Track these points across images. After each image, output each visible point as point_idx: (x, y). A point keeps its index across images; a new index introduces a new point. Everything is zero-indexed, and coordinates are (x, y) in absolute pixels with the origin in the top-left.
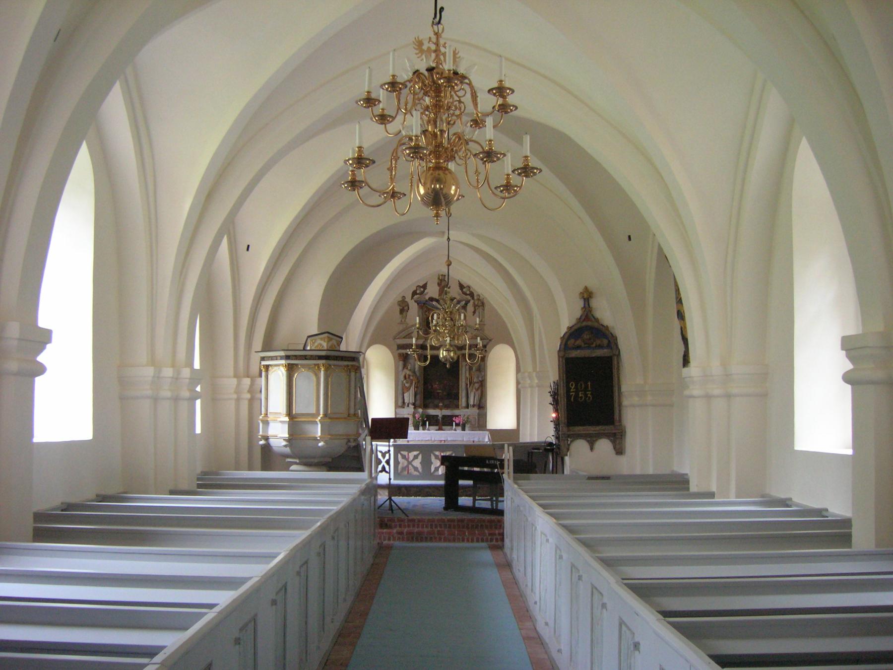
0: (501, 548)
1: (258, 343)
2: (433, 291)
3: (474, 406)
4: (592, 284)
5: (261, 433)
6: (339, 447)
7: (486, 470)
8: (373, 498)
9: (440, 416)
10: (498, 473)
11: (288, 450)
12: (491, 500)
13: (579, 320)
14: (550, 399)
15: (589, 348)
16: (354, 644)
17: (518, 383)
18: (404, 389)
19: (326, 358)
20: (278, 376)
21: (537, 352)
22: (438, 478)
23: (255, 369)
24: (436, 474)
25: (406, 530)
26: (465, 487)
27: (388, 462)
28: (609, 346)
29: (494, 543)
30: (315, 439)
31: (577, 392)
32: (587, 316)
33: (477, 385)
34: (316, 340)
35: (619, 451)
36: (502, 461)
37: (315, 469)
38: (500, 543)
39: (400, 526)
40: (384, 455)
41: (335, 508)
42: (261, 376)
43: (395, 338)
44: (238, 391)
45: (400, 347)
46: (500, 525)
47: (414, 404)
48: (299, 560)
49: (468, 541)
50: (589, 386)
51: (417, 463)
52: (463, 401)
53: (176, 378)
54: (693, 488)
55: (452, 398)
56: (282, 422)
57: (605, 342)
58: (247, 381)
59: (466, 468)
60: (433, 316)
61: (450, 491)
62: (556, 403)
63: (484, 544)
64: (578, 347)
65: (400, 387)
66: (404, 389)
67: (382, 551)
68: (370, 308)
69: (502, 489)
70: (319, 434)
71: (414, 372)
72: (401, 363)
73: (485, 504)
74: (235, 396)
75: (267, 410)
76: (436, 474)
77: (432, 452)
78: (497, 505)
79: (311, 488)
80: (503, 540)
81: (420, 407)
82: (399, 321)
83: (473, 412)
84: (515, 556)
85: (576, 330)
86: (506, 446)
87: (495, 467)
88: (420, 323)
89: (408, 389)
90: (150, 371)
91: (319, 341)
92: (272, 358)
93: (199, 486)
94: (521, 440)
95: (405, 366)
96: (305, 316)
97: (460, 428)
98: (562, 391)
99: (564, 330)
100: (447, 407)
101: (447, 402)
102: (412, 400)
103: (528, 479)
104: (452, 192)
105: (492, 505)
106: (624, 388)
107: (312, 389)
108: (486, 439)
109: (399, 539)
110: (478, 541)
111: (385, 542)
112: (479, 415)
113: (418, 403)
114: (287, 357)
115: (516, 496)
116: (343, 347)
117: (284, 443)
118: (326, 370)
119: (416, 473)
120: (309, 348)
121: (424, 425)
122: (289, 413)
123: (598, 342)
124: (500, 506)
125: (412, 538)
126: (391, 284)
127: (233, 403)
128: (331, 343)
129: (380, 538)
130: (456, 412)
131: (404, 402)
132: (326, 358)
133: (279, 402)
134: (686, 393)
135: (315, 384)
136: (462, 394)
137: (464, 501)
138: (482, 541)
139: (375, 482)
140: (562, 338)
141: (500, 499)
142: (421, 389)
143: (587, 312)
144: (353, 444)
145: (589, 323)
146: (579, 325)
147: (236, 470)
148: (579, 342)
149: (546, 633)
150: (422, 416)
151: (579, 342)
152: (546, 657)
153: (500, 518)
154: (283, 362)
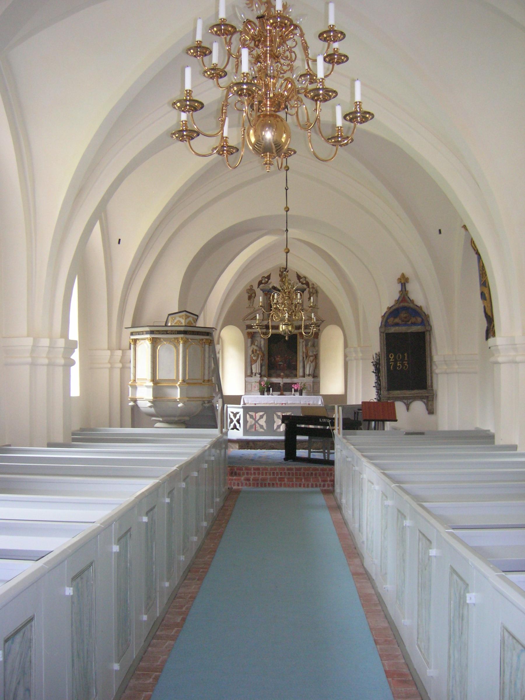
0: (332, 492)
1: (128, 321)
2: (275, 281)
3: (309, 375)
4: (409, 273)
5: (130, 396)
6: (196, 407)
7: (319, 427)
8: (223, 451)
9: (282, 384)
10: (329, 430)
11: (152, 410)
12: (324, 452)
13: (397, 301)
14: (373, 368)
15: (405, 325)
16: (201, 579)
17: (346, 356)
18: (252, 362)
19: (185, 332)
20: (144, 348)
21: (361, 329)
22: (279, 434)
23: (125, 342)
24: (278, 430)
25: (252, 477)
26: (302, 442)
27: (238, 421)
28: (422, 323)
29: (326, 488)
30: (175, 401)
31: (395, 361)
32: (404, 297)
33: (311, 358)
34: (175, 319)
35: (431, 411)
36: (333, 419)
37: (176, 426)
38: (331, 488)
39: (247, 474)
40: (235, 415)
41: (185, 459)
42: (130, 349)
44: (111, 362)
46: (331, 473)
47: (260, 374)
48: (148, 502)
49: (304, 486)
50: (406, 357)
51: (262, 422)
52: (300, 372)
53: (52, 347)
54: (499, 441)
55: (291, 369)
56: (148, 387)
57: (419, 320)
58: (119, 353)
59: (303, 426)
60: (273, 296)
61: (290, 445)
62: (377, 371)
63: (318, 489)
64: (397, 324)
65: (249, 360)
66: (252, 362)
67: (232, 495)
68: (224, 294)
69: (333, 444)
70: (179, 397)
73: (318, 455)
74: (109, 366)
75: (135, 376)
76: (278, 430)
77: (275, 413)
78: (328, 456)
79: (175, 442)
80: (333, 485)
82: (248, 305)
83: (308, 380)
84: (344, 501)
85: (395, 310)
86: (336, 407)
87: (327, 424)
88: (263, 302)
89: (255, 361)
90: (30, 341)
91: (178, 319)
92: (139, 333)
93: (74, 440)
94: (349, 403)
95: (252, 343)
96: (166, 299)
97: (298, 393)
98: (383, 362)
99: (384, 310)
100: (287, 376)
101: (287, 372)
102: (258, 371)
103: (355, 434)
104: (283, 140)
105: (324, 456)
106: (436, 358)
107: (173, 360)
108: (319, 402)
109: (246, 484)
110: (312, 486)
111: (235, 487)
112: (313, 382)
113: (263, 373)
114: (152, 332)
115: (346, 448)
116: (200, 323)
117: (150, 404)
118: (185, 343)
119: (262, 430)
120: (169, 324)
121: (268, 391)
122: (154, 379)
123: (413, 320)
124: (331, 458)
125: (258, 484)
127: (107, 371)
128: (188, 320)
129: (230, 484)
130: (295, 380)
131: (252, 373)
132: (185, 332)
133: (146, 371)
134: (492, 359)
135: (175, 354)
136: (300, 366)
137: (301, 453)
138: (316, 486)
139: (225, 437)
140: (383, 317)
141: (331, 451)
142: (266, 361)
143: (404, 292)
144: (207, 405)
145: (406, 304)
146: (397, 306)
147: (110, 427)
148: (397, 320)
149: (373, 570)
150: (266, 383)
151: (397, 320)
152: (373, 592)
153: (330, 467)
154: (148, 336)
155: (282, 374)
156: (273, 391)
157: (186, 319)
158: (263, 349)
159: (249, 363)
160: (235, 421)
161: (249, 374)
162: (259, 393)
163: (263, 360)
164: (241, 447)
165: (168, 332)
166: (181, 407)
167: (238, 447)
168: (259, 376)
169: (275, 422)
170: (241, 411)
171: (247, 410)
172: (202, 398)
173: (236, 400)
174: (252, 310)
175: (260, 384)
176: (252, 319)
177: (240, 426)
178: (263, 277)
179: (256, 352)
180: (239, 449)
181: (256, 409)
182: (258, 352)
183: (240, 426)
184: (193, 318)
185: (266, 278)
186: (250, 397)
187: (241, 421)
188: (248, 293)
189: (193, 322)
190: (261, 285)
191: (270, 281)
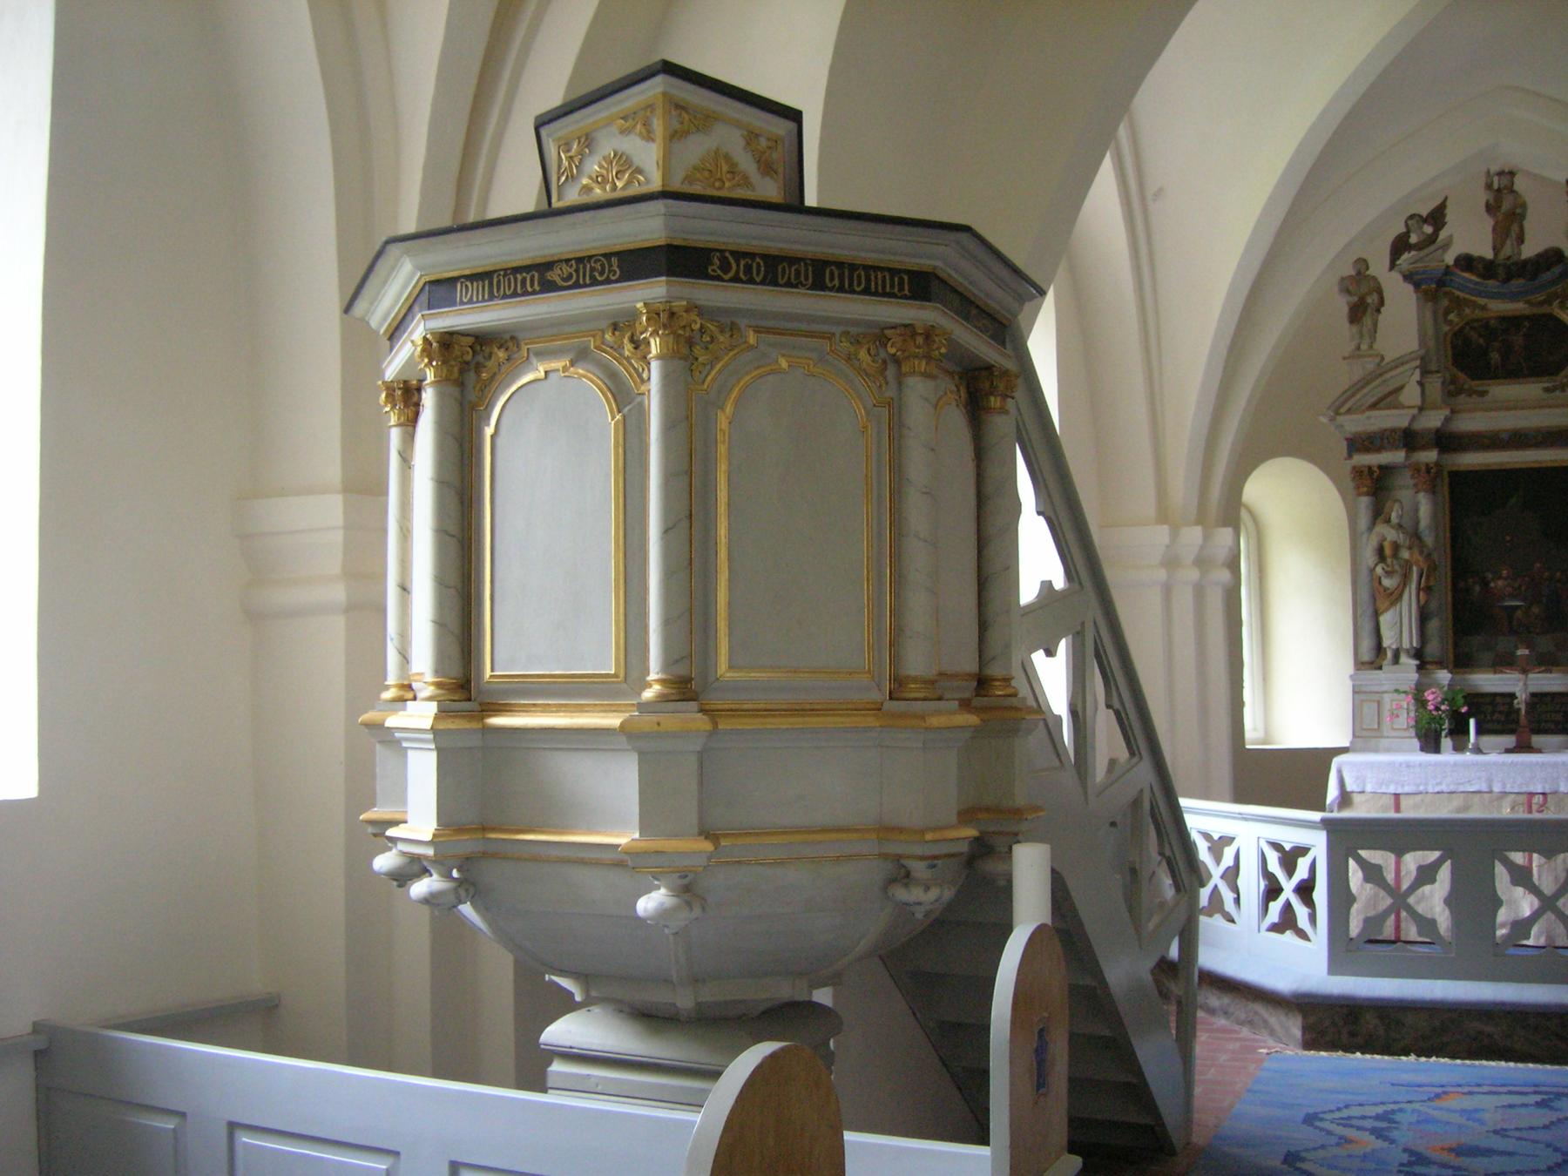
19: (680, 260)
34: (588, 141)
43: (1337, 410)
45: (1358, 444)
47: (1418, 654)
51: (1434, 900)
65: (1365, 595)
71: (1416, 535)
72: (1364, 502)
81: (1441, 664)
82: (1349, 348)
89: (1395, 597)
101: (1545, 643)
102: (1410, 640)
113: (1433, 648)
121: (1459, 731)
126: (1302, 190)
128: (696, 148)
131: (1379, 649)
132: (680, 260)
155: (1522, 652)
156: (1479, 732)
157: (673, 136)
158: (1429, 540)
159: (1370, 603)
160: (1288, 886)
161: (1372, 655)
162: (1416, 743)
163: (1428, 589)
164: (1315, 1039)
165: (554, 275)
166: (663, 914)
167: (1297, 1032)
168: (1415, 662)
169: (1497, 903)
170: (1318, 842)
171: (1347, 837)
172: (886, 830)
173: (1289, 778)
174: (1370, 366)
175: (1421, 702)
176: (1374, 406)
177: (1313, 918)
178: (1412, 217)
179: (1395, 555)
180: (1308, 1045)
181: (1397, 834)
182: (1405, 554)
183: (1313, 918)
184: (752, 137)
185: (1425, 221)
186: (1371, 765)
187: (1320, 894)
188: (1348, 292)
189: (746, 164)
190: (1406, 256)
191: (1443, 234)
